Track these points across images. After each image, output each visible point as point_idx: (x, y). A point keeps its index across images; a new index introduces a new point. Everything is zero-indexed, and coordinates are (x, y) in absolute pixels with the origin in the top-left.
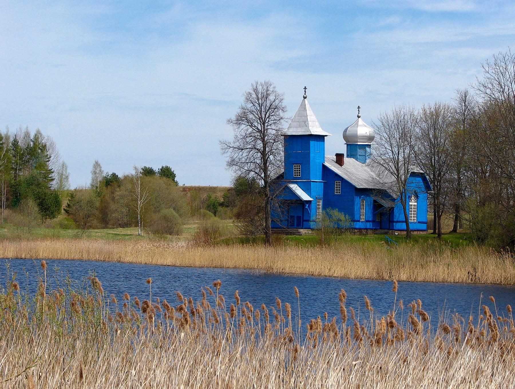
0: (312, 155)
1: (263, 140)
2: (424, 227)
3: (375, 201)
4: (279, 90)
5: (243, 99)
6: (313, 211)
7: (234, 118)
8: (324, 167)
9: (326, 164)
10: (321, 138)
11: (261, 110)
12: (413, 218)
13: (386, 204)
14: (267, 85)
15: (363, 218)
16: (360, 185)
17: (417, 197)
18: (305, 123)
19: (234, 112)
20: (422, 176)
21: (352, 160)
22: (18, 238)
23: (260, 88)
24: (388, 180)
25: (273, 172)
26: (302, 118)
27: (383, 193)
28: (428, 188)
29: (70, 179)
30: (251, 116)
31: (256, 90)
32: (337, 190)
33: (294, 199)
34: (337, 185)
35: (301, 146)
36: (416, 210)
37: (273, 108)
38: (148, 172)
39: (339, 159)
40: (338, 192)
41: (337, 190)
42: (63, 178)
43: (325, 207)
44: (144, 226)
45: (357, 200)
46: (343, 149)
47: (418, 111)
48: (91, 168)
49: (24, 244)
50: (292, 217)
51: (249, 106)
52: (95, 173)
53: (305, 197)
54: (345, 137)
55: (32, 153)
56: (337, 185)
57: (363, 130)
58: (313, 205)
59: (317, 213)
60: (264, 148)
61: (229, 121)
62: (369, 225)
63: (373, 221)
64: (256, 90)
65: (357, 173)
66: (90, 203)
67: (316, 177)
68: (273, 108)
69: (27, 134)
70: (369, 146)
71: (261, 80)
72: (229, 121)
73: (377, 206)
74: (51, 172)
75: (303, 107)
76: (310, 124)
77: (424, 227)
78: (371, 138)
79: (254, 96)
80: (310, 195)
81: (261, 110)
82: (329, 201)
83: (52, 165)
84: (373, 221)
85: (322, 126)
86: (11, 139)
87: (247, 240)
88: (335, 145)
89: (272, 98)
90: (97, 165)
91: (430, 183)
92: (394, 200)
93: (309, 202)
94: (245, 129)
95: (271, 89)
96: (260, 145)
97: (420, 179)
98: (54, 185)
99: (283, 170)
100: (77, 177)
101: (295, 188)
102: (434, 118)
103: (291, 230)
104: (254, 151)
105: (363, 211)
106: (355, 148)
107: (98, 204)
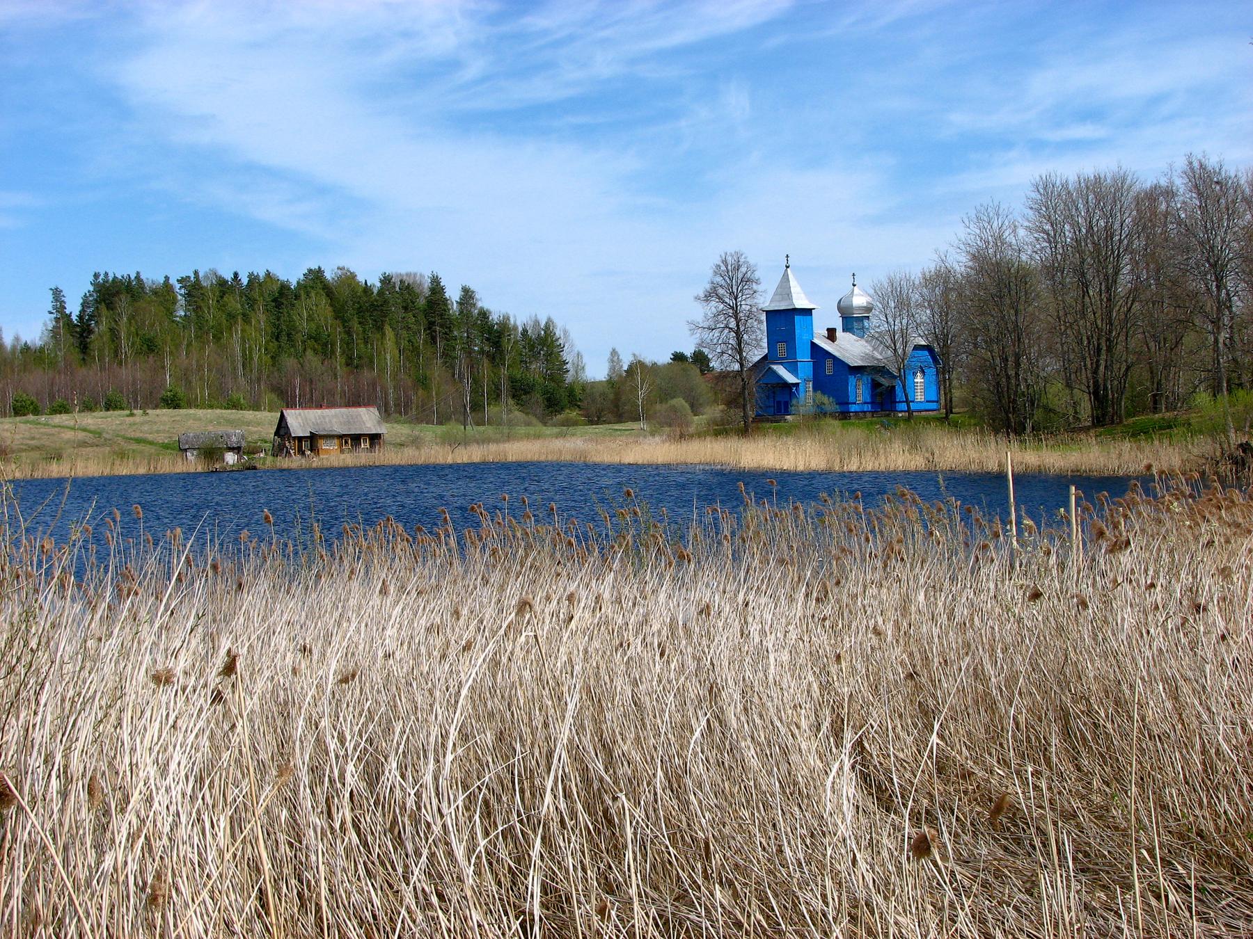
0: (797, 332)
1: (736, 318)
2: (934, 406)
3: (873, 380)
4: (752, 261)
5: (711, 272)
6: (802, 395)
7: (702, 295)
8: (813, 344)
9: (816, 341)
10: (808, 312)
11: (731, 283)
12: (920, 397)
13: (885, 382)
14: (738, 255)
15: (860, 399)
16: (855, 362)
17: (923, 372)
18: (789, 295)
19: (702, 288)
20: (928, 348)
21: (848, 335)
22: (486, 440)
23: (729, 259)
24: (881, 356)
25: (755, 354)
26: (784, 289)
27: (880, 370)
28: (935, 360)
29: (587, 368)
30: (721, 291)
31: (725, 262)
32: (829, 369)
33: (774, 381)
34: (829, 363)
35: (784, 321)
36: (920, 388)
37: (746, 280)
38: (678, 357)
39: (831, 334)
40: (830, 373)
41: (829, 369)
42: (580, 368)
43: (815, 389)
44: (648, 418)
45: (852, 380)
46: (837, 323)
47: (916, 275)
48: (609, 355)
49: (493, 447)
50: (779, 403)
51: (719, 279)
52: (612, 361)
53: (790, 378)
54: (839, 309)
55: (544, 344)
56: (829, 363)
57: (859, 300)
58: (801, 387)
59: (807, 397)
60: (738, 326)
61: (697, 298)
62: (867, 408)
63: (871, 403)
64: (725, 262)
65: (851, 349)
66: (603, 394)
67: (804, 356)
68: (746, 280)
69: (537, 322)
70: (868, 317)
71: (731, 250)
72: (697, 298)
73: (875, 385)
74: (565, 363)
75: (785, 278)
76: (794, 296)
77: (934, 406)
78: (869, 309)
79: (723, 268)
80: (797, 376)
81: (731, 283)
82: (820, 383)
83: (567, 356)
84: (871, 403)
85: (809, 295)
86: (520, 329)
87: (720, 430)
88: (826, 318)
89: (743, 269)
90: (614, 353)
91: (938, 355)
92: (894, 377)
93: (797, 385)
94: (715, 306)
95: (742, 260)
96: (733, 324)
97: (926, 353)
98: (569, 377)
99: (766, 351)
100: (596, 371)
101: (781, 371)
102: (941, 280)
103: (778, 417)
104: (726, 331)
105: (859, 393)
106: (852, 320)
107: (611, 396)
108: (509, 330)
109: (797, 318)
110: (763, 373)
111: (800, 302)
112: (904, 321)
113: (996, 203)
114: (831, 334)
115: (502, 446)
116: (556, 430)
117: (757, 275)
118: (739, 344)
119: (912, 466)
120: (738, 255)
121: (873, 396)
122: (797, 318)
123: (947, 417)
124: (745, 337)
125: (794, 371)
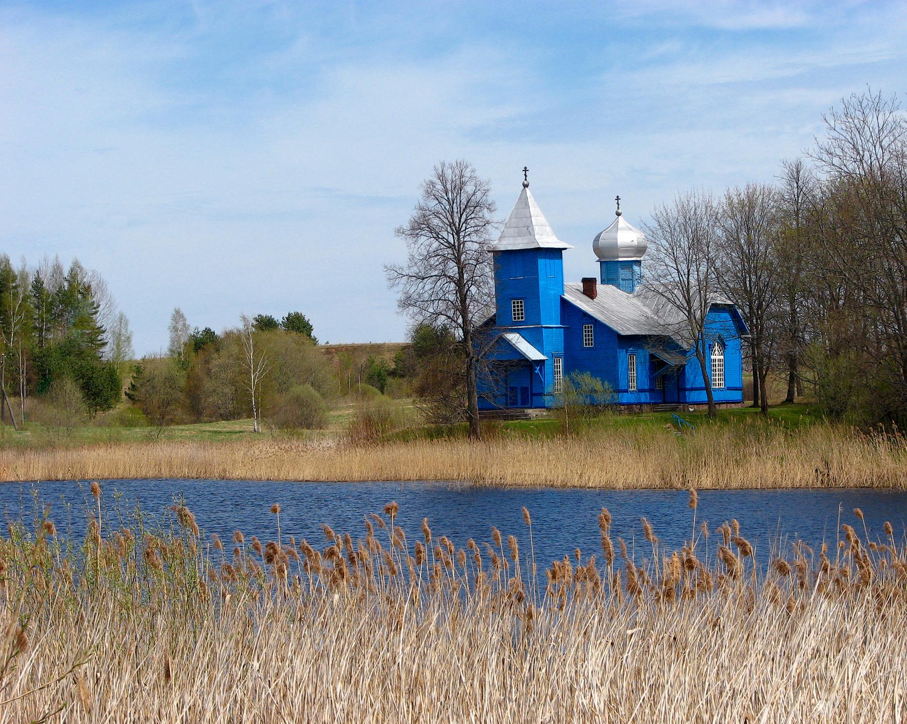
0: (542, 283)
1: (458, 261)
2: (737, 395)
3: (652, 356)
4: (482, 175)
6: (548, 377)
7: (406, 226)
8: (564, 302)
9: (567, 297)
10: (556, 253)
11: (451, 210)
12: (718, 382)
13: (672, 360)
14: (461, 167)
17: (723, 345)
18: (528, 229)
19: (407, 216)
21: (610, 288)
22: (50, 446)
23: (449, 173)
24: (673, 319)
25: (478, 315)
27: (665, 342)
28: (741, 329)
29: (134, 341)
30: (435, 221)
31: (442, 177)
32: (588, 340)
35: (522, 267)
38: (266, 324)
39: (589, 288)
40: (589, 343)
41: (588, 340)
42: (123, 340)
43: (568, 369)
45: (623, 355)
46: (594, 271)
47: (719, 200)
48: (168, 321)
49: (60, 456)
51: (432, 203)
52: (175, 329)
53: (533, 354)
54: (597, 250)
55: (70, 299)
57: (627, 236)
58: (548, 368)
59: (556, 381)
60: (461, 273)
61: (400, 232)
62: (644, 398)
63: (651, 390)
64: (442, 177)
65: (619, 309)
66: (170, 380)
67: (551, 319)
68: (473, 206)
69: (57, 269)
71: (451, 160)
73: (656, 364)
74: (100, 331)
75: (523, 202)
76: (536, 229)
77: (737, 395)
78: (641, 250)
79: (439, 186)
80: (541, 351)
81: (451, 210)
82: (574, 361)
84: (651, 390)
86: (31, 279)
87: (438, 431)
88: (580, 264)
90: (178, 316)
91: (745, 321)
92: (684, 352)
93: (541, 362)
94: (426, 243)
95: (467, 174)
97: (727, 316)
98: (107, 353)
102: (746, 210)
103: (512, 412)
105: (633, 374)
106: (614, 267)
107: (182, 382)
108: (14, 278)
109: (542, 262)
110: (494, 349)
111: (547, 240)
112: (703, 269)
113: (875, 93)
114: (589, 288)
115: (74, 455)
116: (104, 432)
117: (490, 198)
118: (463, 301)
119: (644, 481)
120: (461, 167)
121: (652, 380)
122: (542, 262)
123: (756, 411)
124: (473, 289)
125: (536, 342)
